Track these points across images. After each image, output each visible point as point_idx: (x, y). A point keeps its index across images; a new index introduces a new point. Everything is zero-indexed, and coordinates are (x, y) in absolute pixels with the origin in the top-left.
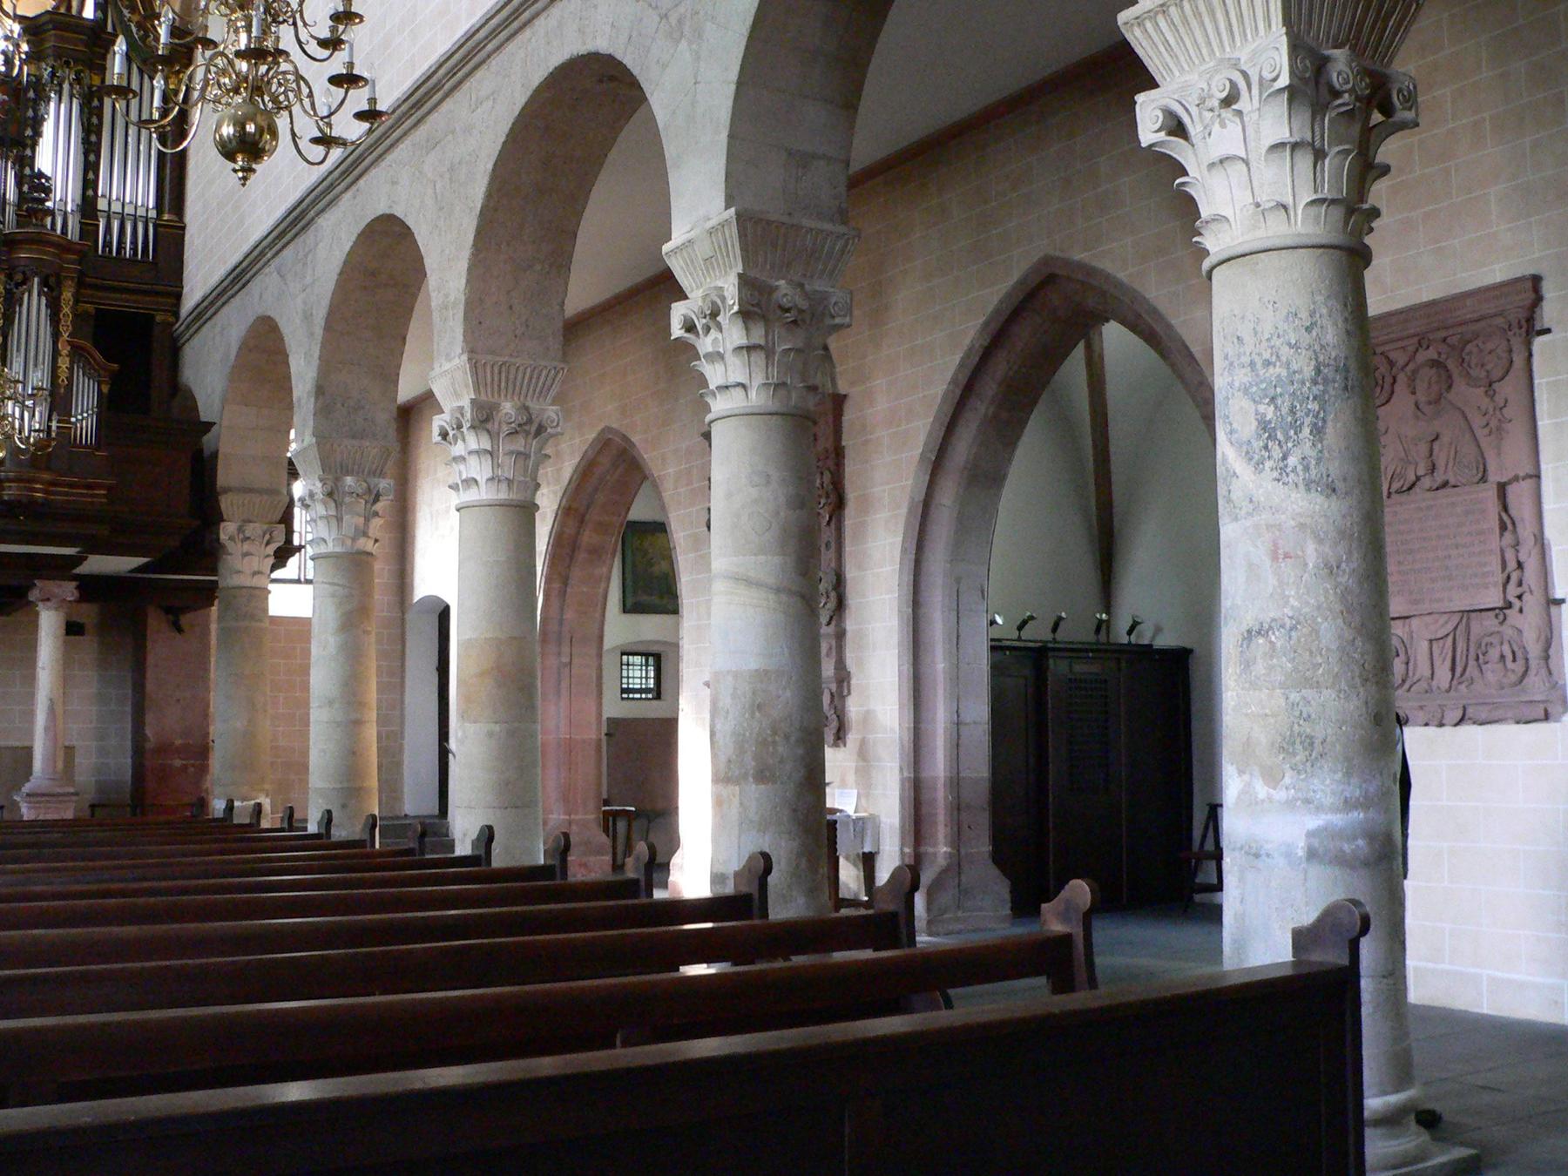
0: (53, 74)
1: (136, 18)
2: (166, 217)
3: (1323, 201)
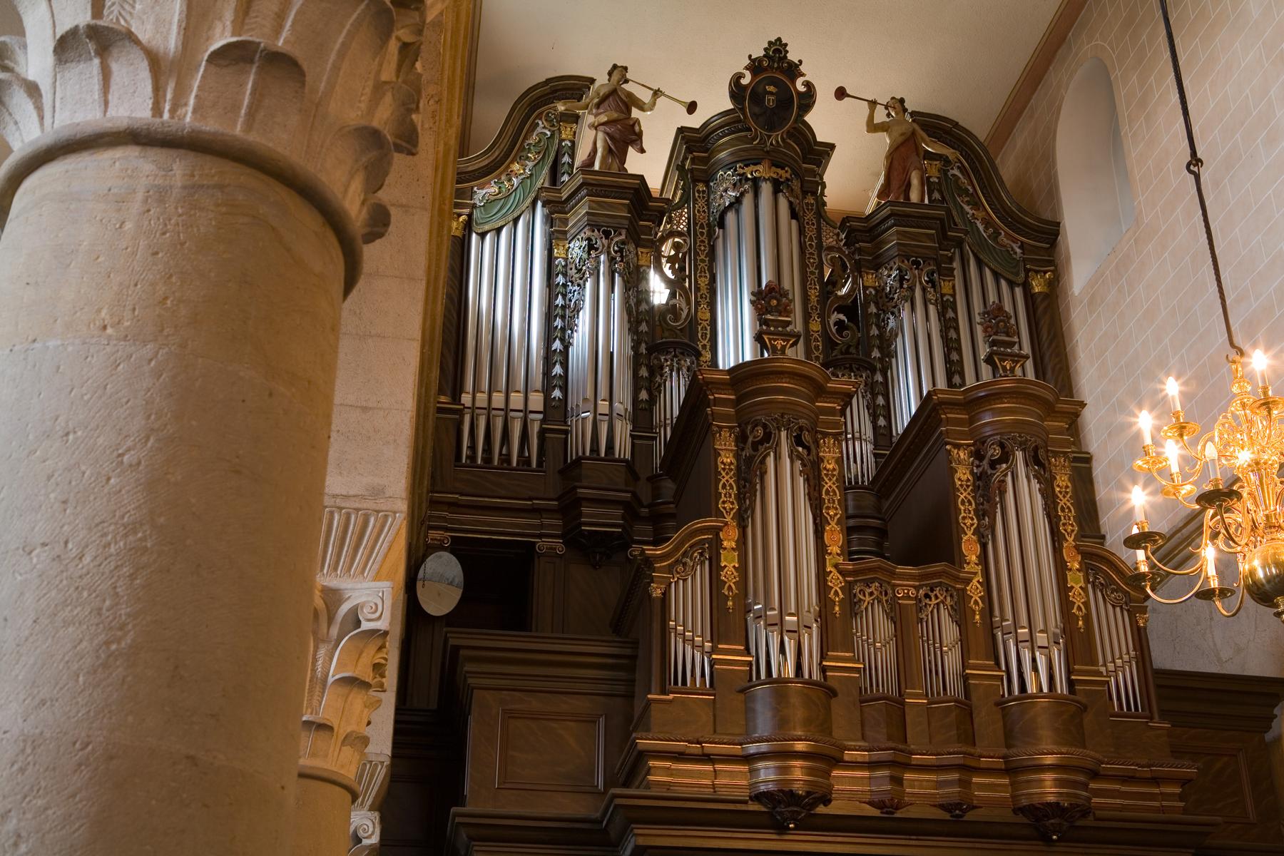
0: (901, 279)
1: (980, 214)
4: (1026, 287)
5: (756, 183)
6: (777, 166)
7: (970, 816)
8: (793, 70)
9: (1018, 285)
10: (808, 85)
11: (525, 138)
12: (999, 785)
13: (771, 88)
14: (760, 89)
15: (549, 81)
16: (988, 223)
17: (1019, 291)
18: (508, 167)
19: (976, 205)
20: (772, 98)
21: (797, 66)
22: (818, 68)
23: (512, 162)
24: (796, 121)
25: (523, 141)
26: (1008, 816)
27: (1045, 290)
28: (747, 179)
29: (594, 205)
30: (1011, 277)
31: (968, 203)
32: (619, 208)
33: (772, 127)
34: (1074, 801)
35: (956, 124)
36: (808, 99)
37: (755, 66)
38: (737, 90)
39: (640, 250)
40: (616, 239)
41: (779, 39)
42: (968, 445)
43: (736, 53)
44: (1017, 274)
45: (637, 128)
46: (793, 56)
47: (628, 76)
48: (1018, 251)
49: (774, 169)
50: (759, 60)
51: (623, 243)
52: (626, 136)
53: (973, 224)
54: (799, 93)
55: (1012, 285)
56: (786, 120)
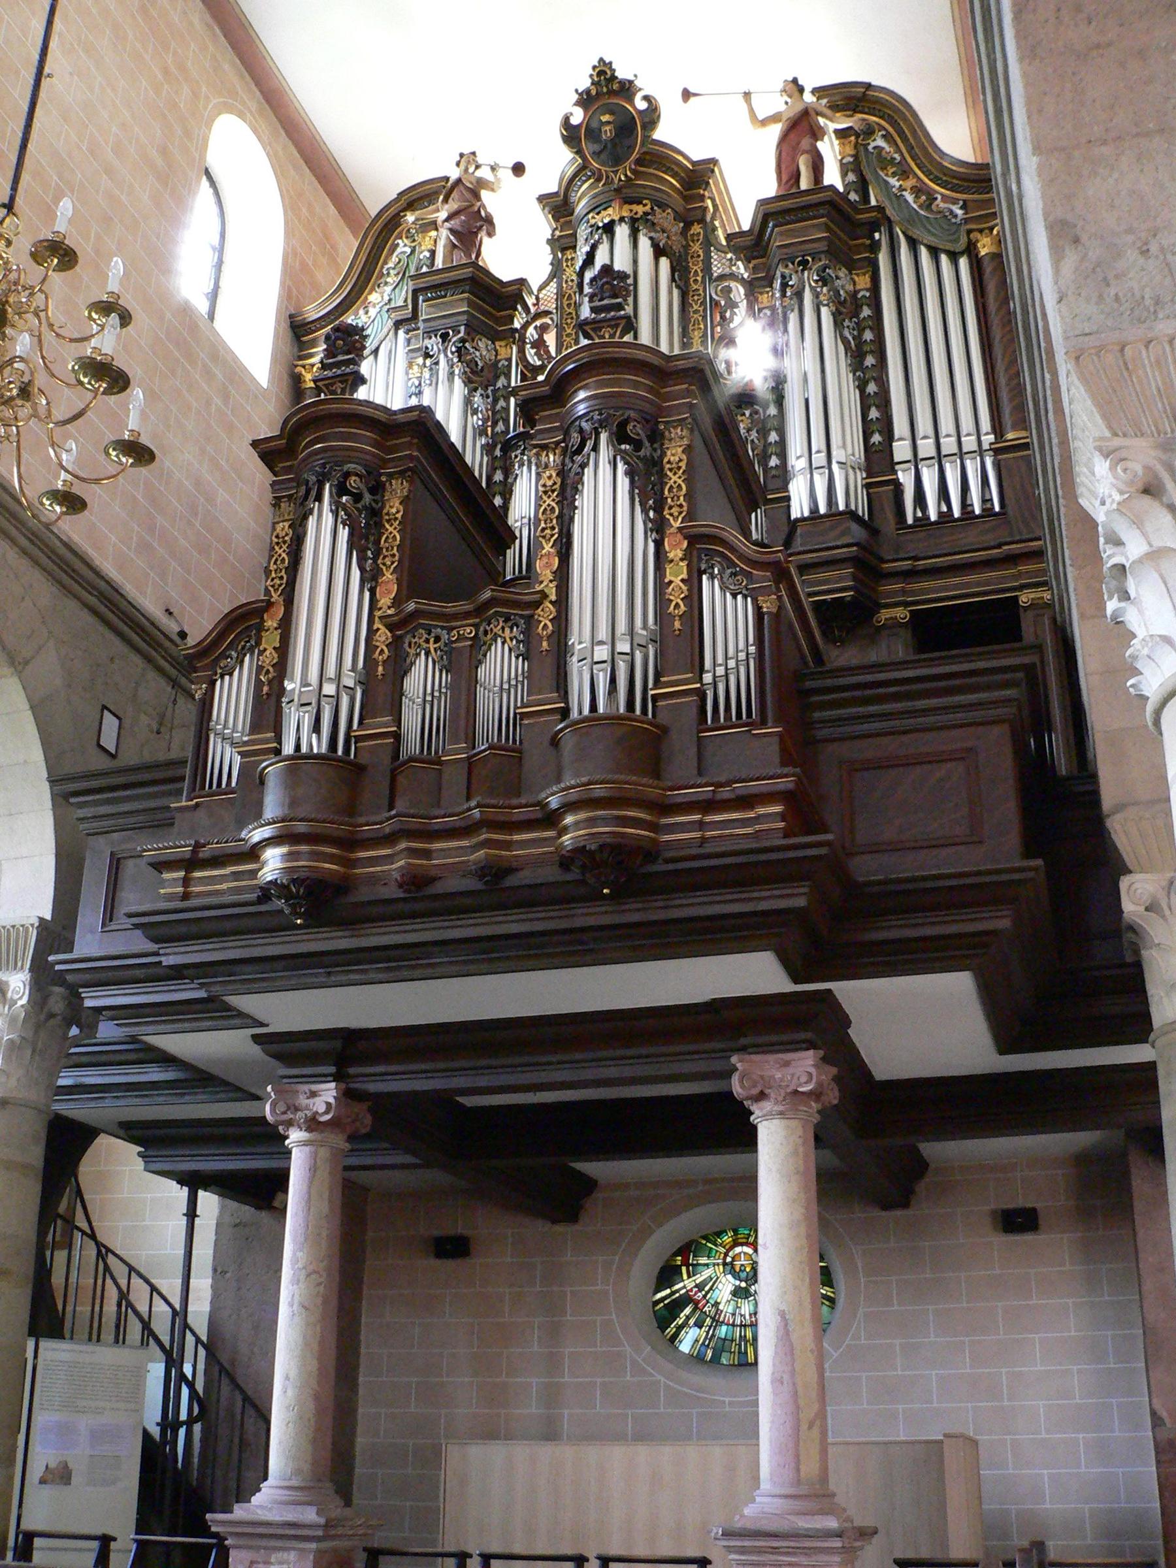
1: (911, 182)
2: (1010, 436)
3: (816, 1496)
4: (971, 250)
5: (609, 229)
6: (631, 203)
7: (511, 881)
8: (627, 89)
9: (962, 253)
10: (646, 98)
11: (385, 263)
12: (545, 839)
13: (605, 118)
14: (594, 125)
15: (401, 194)
16: (917, 191)
17: (963, 262)
18: (366, 298)
19: (904, 174)
20: (608, 128)
21: (631, 82)
22: (652, 77)
23: (370, 293)
24: (643, 144)
25: (382, 267)
26: (551, 873)
27: (994, 249)
28: (598, 228)
29: (432, 310)
30: (949, 247)
31: (894, 174)
32: (458, 305)
33: (617, 161)
34: (601, 841)
35: (869, 86)
36: (651, 116)
37: (585, 100)
38: (571, 135)
39: (497, 343)
40: (455, 339)
41: (601, 60)
42: (557, 443)
43: (561, 96)
44: (957, 241)
45: (483, 214)
46: (622, 73)
47: (480, 162)
48: (960, 212)
49: (626, 207)
50: (588, 92)
51: (463, 341)
52: (473, 225)
53: (900, 198)
54: (640, 112)
55: (954, 257)
56: (631, 148)
